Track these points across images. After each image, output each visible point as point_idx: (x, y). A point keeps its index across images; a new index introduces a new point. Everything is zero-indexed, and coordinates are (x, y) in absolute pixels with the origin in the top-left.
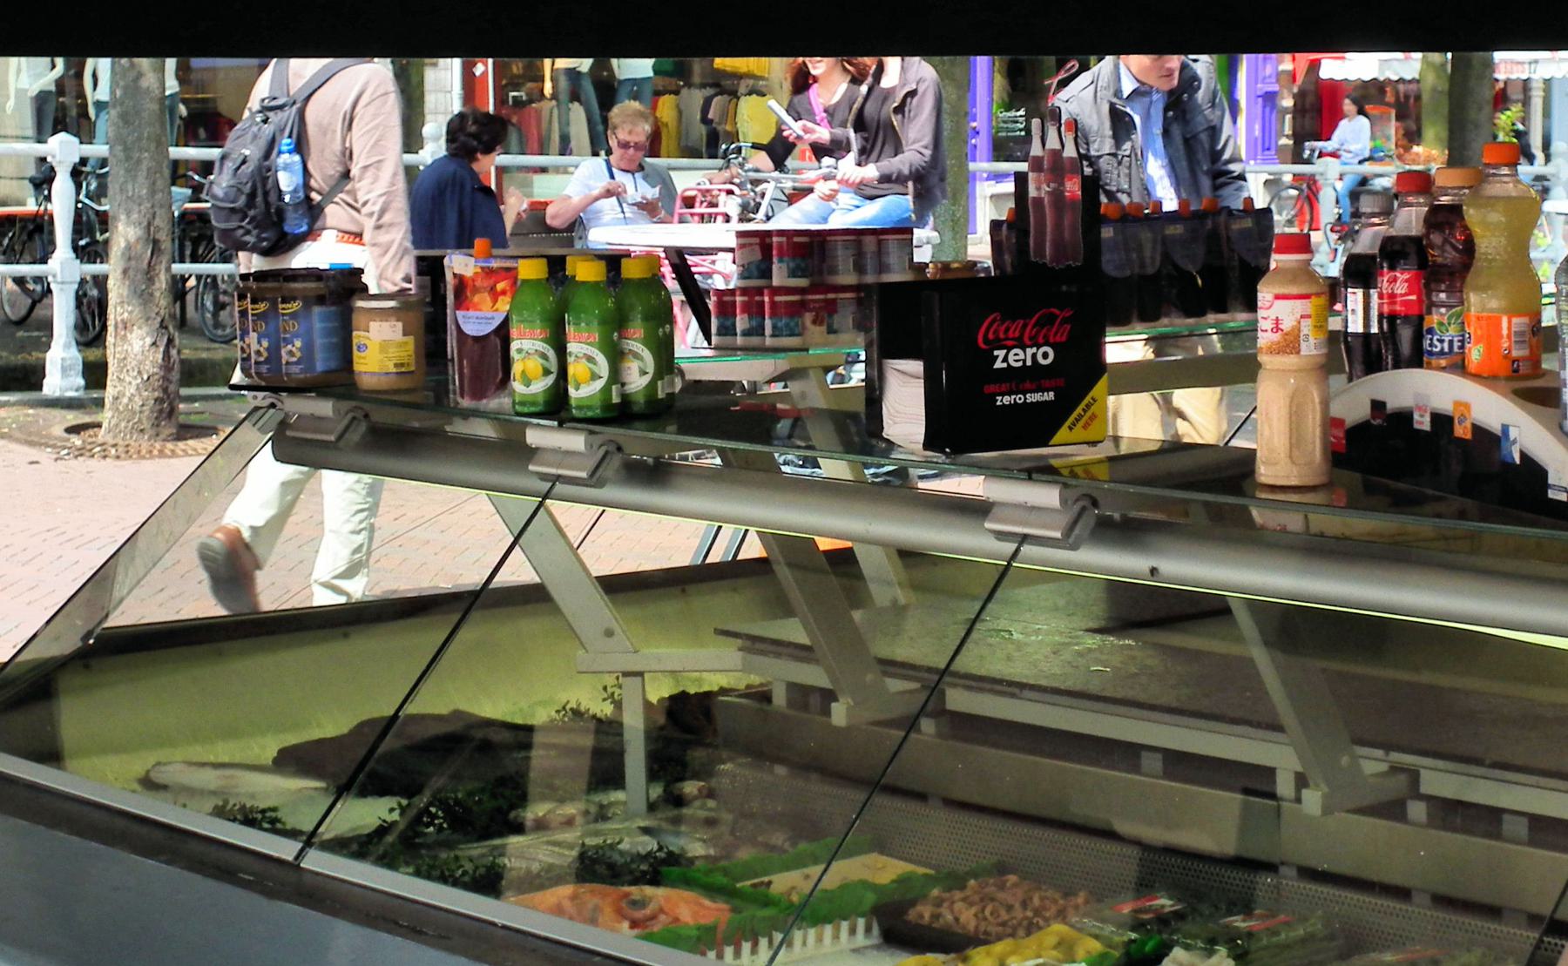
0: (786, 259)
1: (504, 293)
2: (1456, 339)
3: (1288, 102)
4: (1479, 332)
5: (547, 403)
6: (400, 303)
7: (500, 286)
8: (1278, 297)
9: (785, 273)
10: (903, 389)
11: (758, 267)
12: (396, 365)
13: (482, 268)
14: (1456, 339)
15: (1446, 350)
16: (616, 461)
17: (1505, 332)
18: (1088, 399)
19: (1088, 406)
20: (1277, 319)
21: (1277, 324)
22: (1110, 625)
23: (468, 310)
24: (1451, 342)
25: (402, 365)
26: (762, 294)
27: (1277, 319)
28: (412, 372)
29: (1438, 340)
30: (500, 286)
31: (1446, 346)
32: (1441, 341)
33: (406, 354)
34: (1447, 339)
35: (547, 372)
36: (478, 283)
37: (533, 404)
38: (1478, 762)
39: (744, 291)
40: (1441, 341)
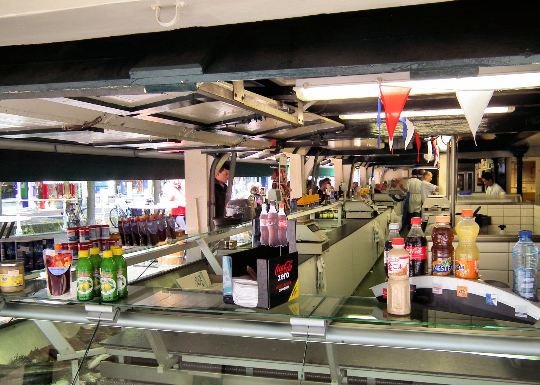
0: (84, 235)
1: (67, 261)
2: (448, 267)
3: (37, 187)
4: (467, 266)
5: (89, 297)
6: (17, 264)
7: (65, 259)
8: (401, 258)
9: (84, 239)
10: (242, 288)
11: (74, 238)
12: (17, 284)
13: (58, 253)
14: (448, 267)
15: (446, 270)
16: (119, 313)
17: (475, 265)
18: (295, 286)
19: (295, 288)
20: (401, 265)
21: (401, 266)
22: (90, 299)
23: (54, 267)
24: (447, 268)
25: (19, 283)
26: (77, 244)
27: (401, 265)
28: (22, 285)
29: (443, 267)
30: (65, 259)
31: (446, 269)
32: (444, 268)
33: (20, 280)
34: (446, 267)
35: (90, 287)
36: (57, 258)
37: (85, 297)
38: (371, 368)
39: (71, 244)
40: (444, 268)
